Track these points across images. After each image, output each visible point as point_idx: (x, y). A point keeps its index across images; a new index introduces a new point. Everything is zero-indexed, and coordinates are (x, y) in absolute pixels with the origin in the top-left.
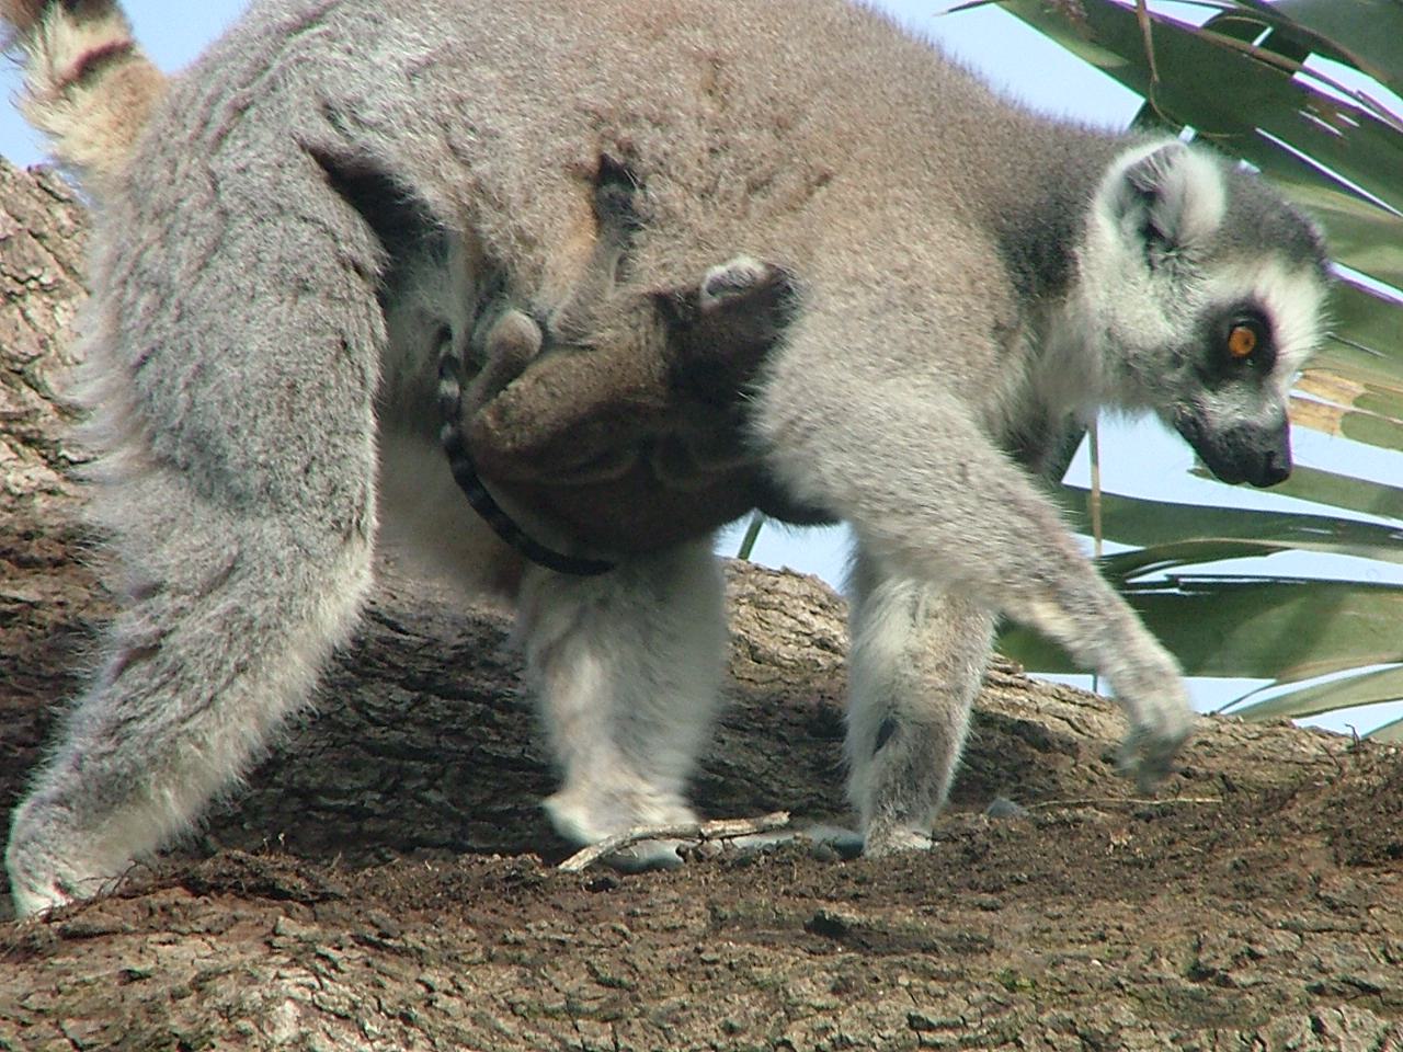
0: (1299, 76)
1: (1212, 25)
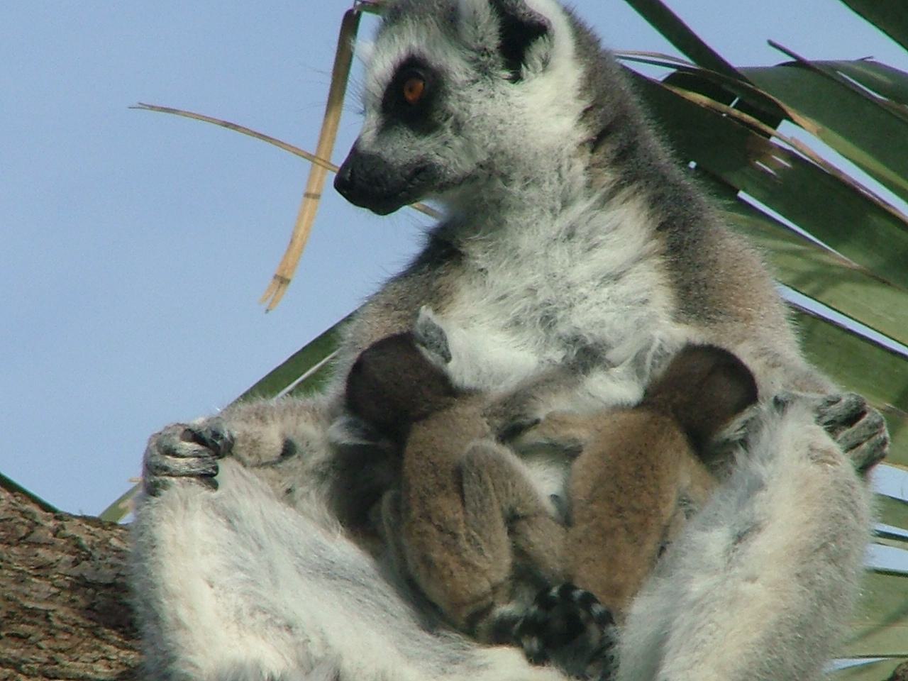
0: (773, 140)
1: (671, 79)
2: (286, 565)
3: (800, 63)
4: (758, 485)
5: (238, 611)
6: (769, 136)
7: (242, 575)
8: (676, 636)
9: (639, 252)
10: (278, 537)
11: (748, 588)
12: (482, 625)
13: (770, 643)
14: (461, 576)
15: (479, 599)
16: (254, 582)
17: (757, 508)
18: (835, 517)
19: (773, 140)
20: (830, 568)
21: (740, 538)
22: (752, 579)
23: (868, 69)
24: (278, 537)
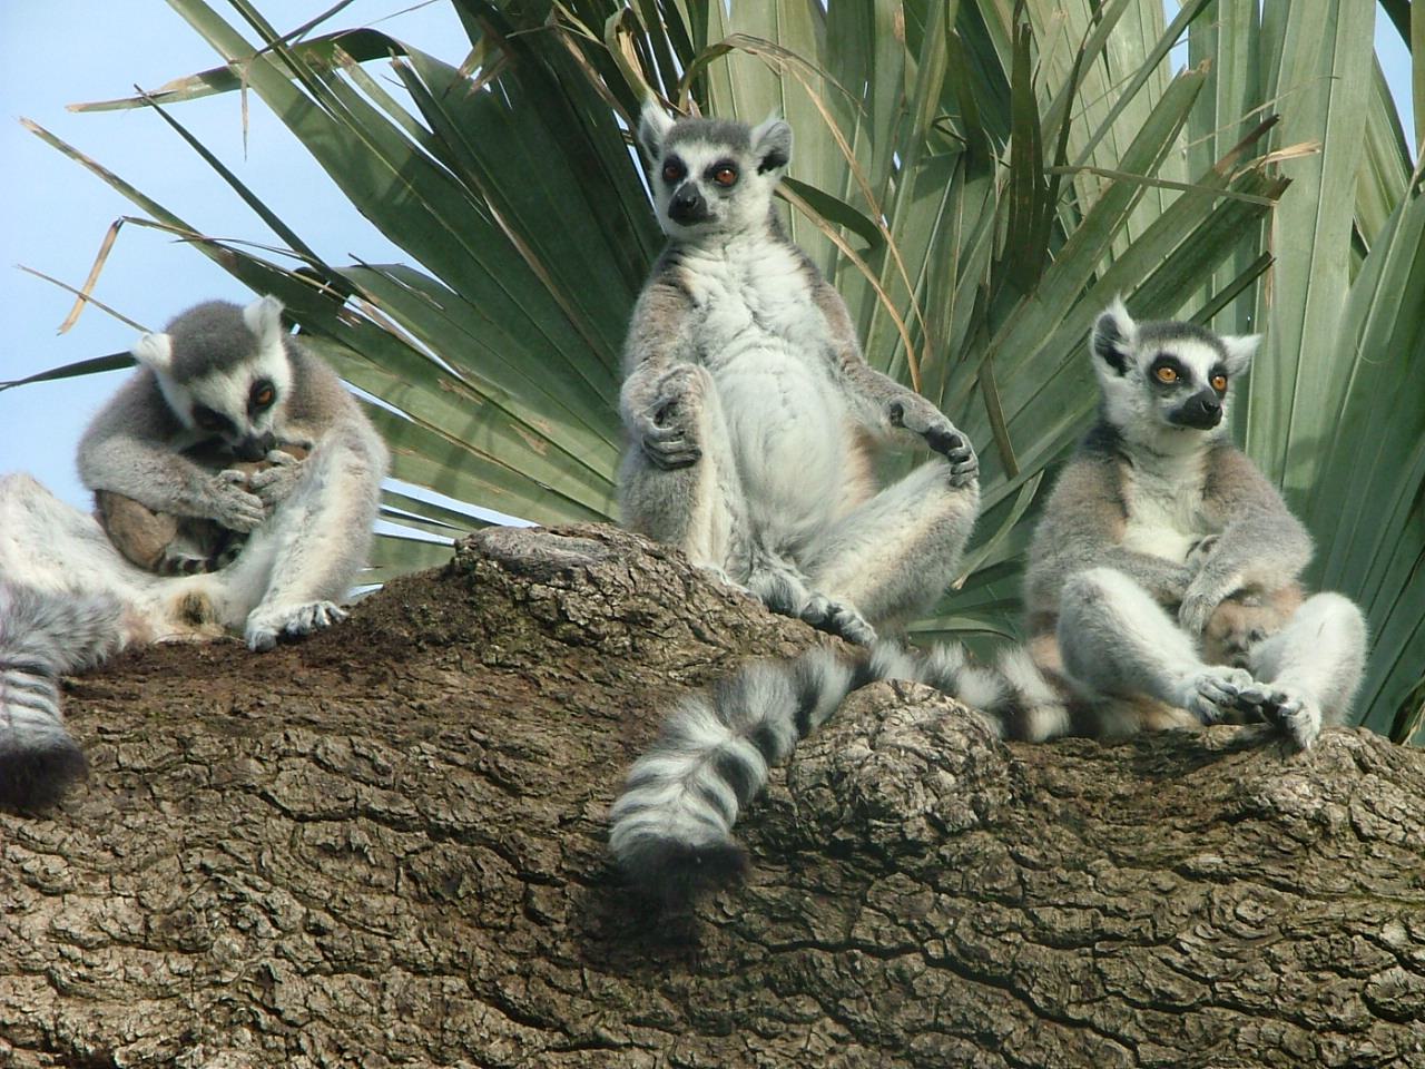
0: (346, 305)
2: (58, 529)
3: (365, 266)
4: (321, 486)
5: (33, 554)
6: (344, 302)
7: (36, 535)
8: (278, 566)
9: (1266, 471)
10: (54, 515)
11: (321, 540)
12: (162, 567)
13: (331, 572)
14: (143, 539)
15: (157, 553)
16: (41, 539)
17: (322, 498)
18: (363, 503)
19: (346, 305)
20: (360, 531)
21: (311, 513)
22: (322, 536)
23: (401, 270)
24: (54, 515)
